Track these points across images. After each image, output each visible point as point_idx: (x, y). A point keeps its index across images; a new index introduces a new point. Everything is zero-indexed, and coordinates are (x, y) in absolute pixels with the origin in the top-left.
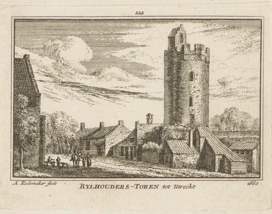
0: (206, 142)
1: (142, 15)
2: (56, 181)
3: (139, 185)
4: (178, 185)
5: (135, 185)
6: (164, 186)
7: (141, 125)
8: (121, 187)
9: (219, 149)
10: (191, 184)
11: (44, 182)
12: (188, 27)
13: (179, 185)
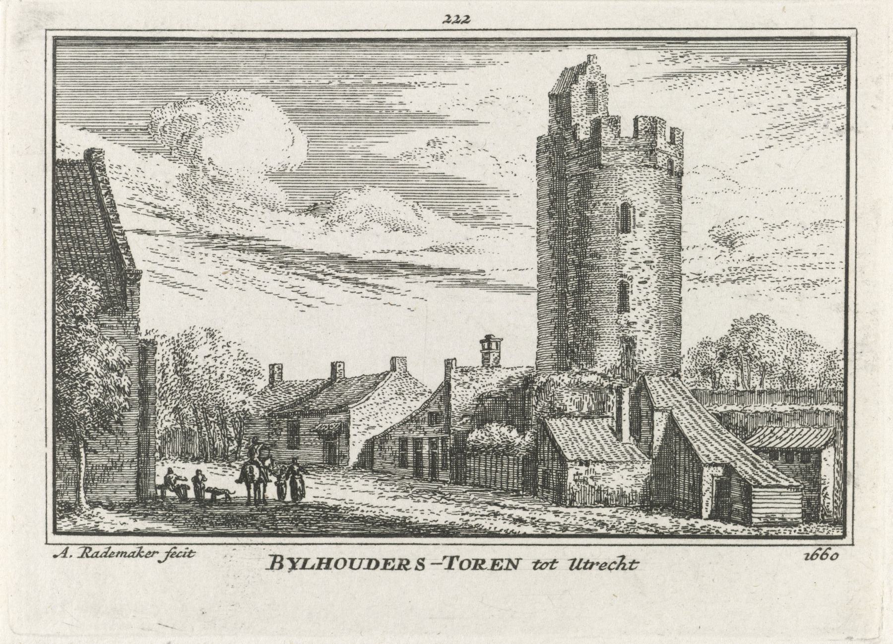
0: (672, 422)
1: (464, 26)
2: (191, 548)
3: (458, 557)
4: (581, 560)
5: (445, 557)
6: (538, 562)
7: (464, 371)
9: (713, 447)
12: (612, 63)
13: (585, 560)
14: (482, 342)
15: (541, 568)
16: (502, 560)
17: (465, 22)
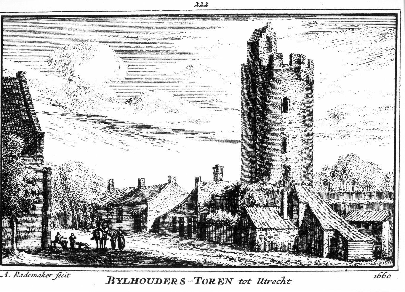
0: (308, 207)
1: (205, 8)
2: (69, 272)
3: (201, 278)
6: (242, 280)
8: (211, 281)
9: (328, 221)
10: (284, 277)
11: (49, 273)
12: (278, 27)
13: (265, 279)
14: (214, 168)
15: (243, 283)
16: (223, 279)
17: (206, 6)
